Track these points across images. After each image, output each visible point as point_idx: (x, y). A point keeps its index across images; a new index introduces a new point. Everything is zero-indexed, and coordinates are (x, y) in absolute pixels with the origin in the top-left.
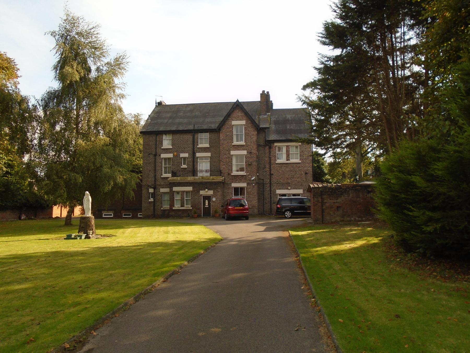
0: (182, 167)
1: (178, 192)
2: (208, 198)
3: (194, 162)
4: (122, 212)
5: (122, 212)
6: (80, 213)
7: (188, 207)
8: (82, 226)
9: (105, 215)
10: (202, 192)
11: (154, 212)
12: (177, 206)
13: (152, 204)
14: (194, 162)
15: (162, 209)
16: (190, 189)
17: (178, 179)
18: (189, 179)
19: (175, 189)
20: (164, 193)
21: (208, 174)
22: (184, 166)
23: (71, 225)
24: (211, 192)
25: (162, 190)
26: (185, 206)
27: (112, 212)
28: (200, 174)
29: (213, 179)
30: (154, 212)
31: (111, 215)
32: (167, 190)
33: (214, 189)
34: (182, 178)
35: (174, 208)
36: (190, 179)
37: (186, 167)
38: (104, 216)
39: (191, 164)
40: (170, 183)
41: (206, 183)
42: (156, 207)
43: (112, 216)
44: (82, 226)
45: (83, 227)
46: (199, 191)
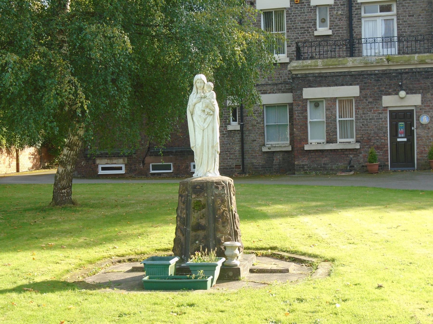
0: (316, 33)
1: (317, 103)
2: (404, 117)
3: (350, 18)
4: (148, 159)
5: (148, 159)
6: (31, 165)
7: (346, 142)
8: (193, 221)
9: (103, 169)
10: (389, 101)
11: (243, 158)
12: (316, 141)
13: (238, 137)
14: (350, 18)
15: (265, 149)
16: (353, 91)
17: (319, 65)
18: (350, 64)
19: (309, 93)
20: (269, 107)
21: (393, 51)
22: (322, 30)
23: (73, 203)
24: (414, 100)
25: (267, 99)
26: (339, 140)
27: (121, 160)
28: (368, 51)
29: (422, 62)
30: (243, 158)
31: (120, 169)
32: (285, 98)
33: (423, 91)
34: (330, 61)
35: (307, 148)
36: (351, 63)
37: (330, 32)
38: (101, 172)
39: (344, 23)
40: (295, 78)
41: (400, 73)
42: (246, 147)
43: (123, 172)
44: (193, 221)
45: (198, 227)
46: (380, 99)
